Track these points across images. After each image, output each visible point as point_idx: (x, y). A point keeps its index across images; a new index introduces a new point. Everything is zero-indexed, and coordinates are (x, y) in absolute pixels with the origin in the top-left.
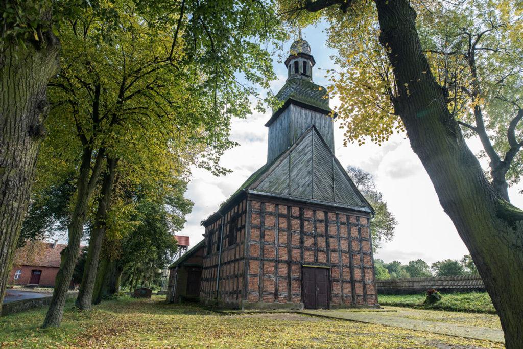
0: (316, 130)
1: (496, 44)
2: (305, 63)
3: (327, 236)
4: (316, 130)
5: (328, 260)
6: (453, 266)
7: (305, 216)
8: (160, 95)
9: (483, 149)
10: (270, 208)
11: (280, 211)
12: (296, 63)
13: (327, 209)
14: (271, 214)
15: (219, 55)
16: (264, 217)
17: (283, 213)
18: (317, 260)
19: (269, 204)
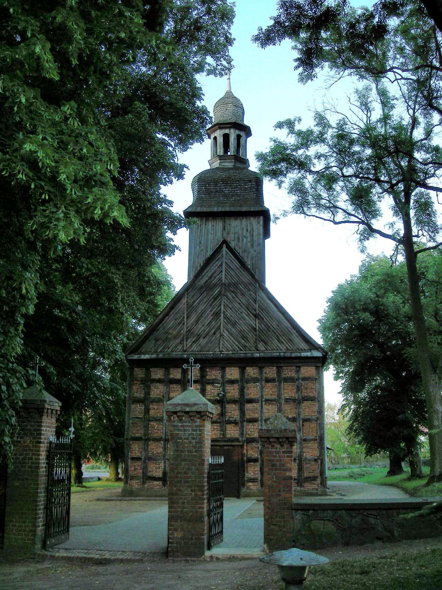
0: (229, 247)
1: (107, 175)
2: (239, 137)
3: (242, 401)
4: (229, 247)
5: (242, 434)
6: (319, 365)
7: (208, 377)
8: (394, 509)
9: (271, 223)
10: (158, 374)
11: (171, 376)
12: (226, 137)
13: (243, 363)
14: (159, 381)
15: (324, 35)
16: (149, 387)
17: (176, 377)
18: (224, 435)
19: (156, 369)
